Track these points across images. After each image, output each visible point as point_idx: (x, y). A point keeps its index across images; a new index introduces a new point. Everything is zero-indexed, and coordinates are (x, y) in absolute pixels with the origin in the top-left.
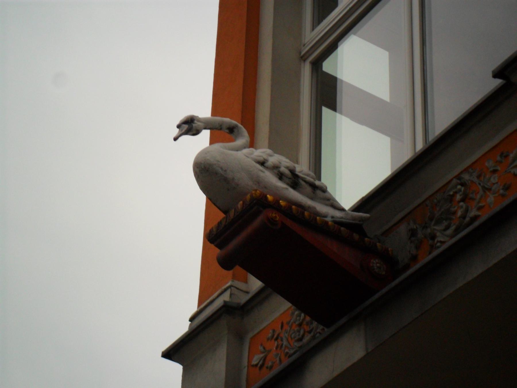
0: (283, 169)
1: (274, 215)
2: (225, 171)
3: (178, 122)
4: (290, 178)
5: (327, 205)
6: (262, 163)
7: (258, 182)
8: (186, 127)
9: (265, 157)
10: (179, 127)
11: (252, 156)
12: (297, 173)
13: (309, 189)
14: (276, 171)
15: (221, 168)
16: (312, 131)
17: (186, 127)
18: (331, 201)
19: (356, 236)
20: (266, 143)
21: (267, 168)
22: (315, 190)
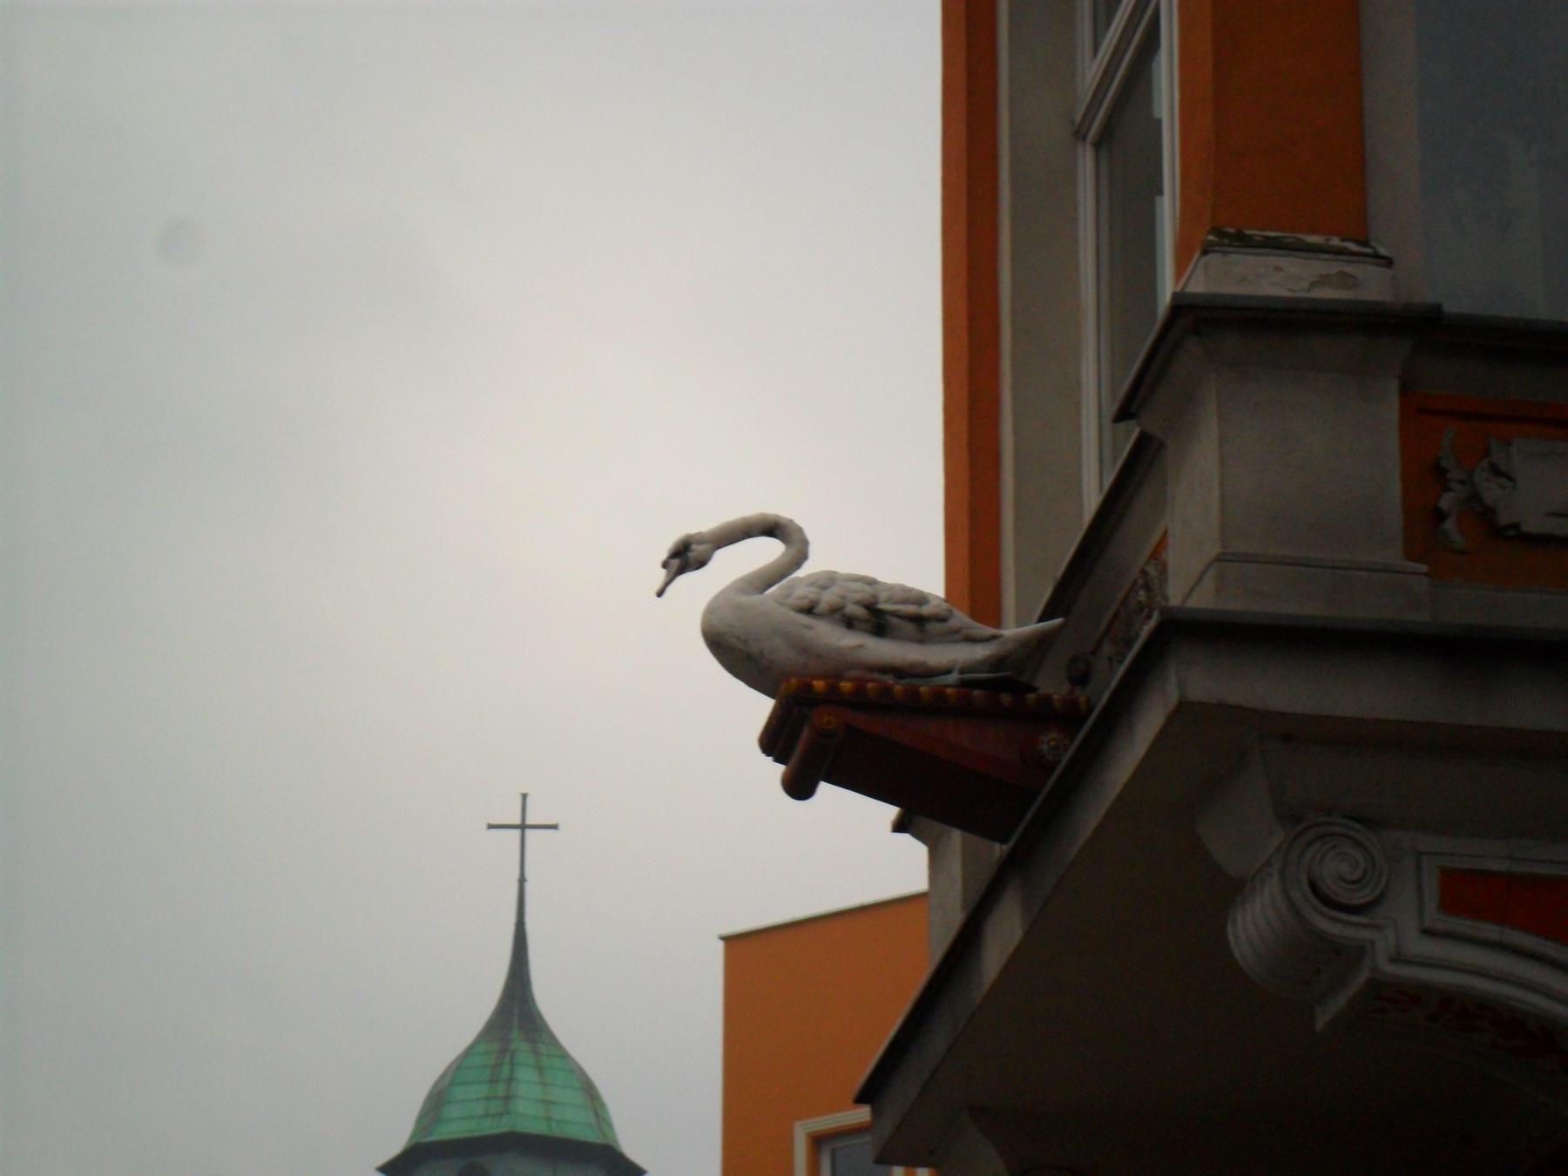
0: (851, 609)
1: (825, 720)
2: (746, 641)
3: (664, 555)
4: (867, 621)
5: (955, 642)
6: (809, 610)
7: (805, 649)
8: (676, 562)
9: (812, 596)
10: (665, 565)
11: (791, 601)
12: (881, 606)
13: (910, 628)
14: (837, 616)
15: (738, 638)
16: (1103, 360)
17: (676, 562)
18: (964, 631)
19: (1006, 698)
20: (1199, 285)
21: (820, 616)
22: (923, 625)
